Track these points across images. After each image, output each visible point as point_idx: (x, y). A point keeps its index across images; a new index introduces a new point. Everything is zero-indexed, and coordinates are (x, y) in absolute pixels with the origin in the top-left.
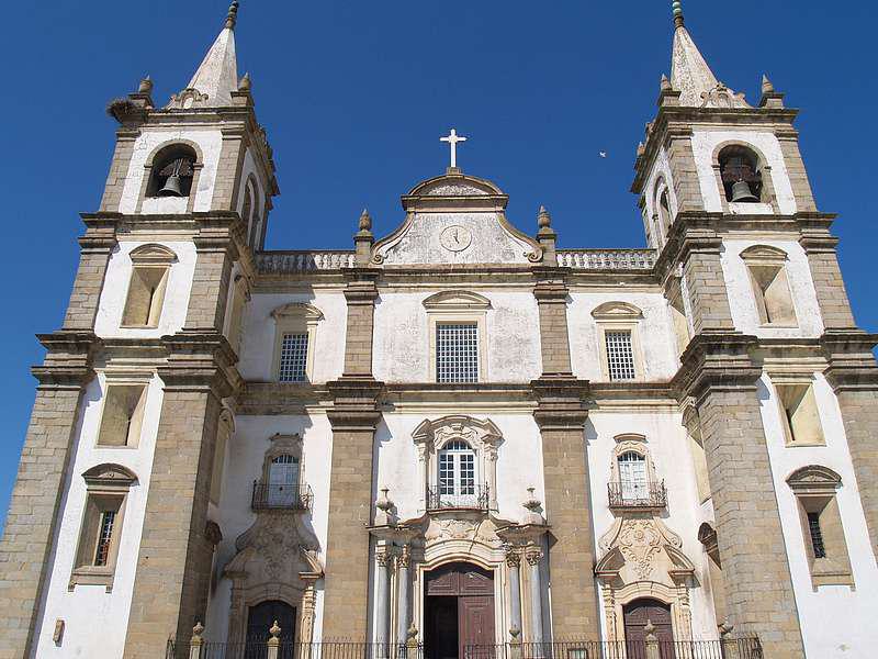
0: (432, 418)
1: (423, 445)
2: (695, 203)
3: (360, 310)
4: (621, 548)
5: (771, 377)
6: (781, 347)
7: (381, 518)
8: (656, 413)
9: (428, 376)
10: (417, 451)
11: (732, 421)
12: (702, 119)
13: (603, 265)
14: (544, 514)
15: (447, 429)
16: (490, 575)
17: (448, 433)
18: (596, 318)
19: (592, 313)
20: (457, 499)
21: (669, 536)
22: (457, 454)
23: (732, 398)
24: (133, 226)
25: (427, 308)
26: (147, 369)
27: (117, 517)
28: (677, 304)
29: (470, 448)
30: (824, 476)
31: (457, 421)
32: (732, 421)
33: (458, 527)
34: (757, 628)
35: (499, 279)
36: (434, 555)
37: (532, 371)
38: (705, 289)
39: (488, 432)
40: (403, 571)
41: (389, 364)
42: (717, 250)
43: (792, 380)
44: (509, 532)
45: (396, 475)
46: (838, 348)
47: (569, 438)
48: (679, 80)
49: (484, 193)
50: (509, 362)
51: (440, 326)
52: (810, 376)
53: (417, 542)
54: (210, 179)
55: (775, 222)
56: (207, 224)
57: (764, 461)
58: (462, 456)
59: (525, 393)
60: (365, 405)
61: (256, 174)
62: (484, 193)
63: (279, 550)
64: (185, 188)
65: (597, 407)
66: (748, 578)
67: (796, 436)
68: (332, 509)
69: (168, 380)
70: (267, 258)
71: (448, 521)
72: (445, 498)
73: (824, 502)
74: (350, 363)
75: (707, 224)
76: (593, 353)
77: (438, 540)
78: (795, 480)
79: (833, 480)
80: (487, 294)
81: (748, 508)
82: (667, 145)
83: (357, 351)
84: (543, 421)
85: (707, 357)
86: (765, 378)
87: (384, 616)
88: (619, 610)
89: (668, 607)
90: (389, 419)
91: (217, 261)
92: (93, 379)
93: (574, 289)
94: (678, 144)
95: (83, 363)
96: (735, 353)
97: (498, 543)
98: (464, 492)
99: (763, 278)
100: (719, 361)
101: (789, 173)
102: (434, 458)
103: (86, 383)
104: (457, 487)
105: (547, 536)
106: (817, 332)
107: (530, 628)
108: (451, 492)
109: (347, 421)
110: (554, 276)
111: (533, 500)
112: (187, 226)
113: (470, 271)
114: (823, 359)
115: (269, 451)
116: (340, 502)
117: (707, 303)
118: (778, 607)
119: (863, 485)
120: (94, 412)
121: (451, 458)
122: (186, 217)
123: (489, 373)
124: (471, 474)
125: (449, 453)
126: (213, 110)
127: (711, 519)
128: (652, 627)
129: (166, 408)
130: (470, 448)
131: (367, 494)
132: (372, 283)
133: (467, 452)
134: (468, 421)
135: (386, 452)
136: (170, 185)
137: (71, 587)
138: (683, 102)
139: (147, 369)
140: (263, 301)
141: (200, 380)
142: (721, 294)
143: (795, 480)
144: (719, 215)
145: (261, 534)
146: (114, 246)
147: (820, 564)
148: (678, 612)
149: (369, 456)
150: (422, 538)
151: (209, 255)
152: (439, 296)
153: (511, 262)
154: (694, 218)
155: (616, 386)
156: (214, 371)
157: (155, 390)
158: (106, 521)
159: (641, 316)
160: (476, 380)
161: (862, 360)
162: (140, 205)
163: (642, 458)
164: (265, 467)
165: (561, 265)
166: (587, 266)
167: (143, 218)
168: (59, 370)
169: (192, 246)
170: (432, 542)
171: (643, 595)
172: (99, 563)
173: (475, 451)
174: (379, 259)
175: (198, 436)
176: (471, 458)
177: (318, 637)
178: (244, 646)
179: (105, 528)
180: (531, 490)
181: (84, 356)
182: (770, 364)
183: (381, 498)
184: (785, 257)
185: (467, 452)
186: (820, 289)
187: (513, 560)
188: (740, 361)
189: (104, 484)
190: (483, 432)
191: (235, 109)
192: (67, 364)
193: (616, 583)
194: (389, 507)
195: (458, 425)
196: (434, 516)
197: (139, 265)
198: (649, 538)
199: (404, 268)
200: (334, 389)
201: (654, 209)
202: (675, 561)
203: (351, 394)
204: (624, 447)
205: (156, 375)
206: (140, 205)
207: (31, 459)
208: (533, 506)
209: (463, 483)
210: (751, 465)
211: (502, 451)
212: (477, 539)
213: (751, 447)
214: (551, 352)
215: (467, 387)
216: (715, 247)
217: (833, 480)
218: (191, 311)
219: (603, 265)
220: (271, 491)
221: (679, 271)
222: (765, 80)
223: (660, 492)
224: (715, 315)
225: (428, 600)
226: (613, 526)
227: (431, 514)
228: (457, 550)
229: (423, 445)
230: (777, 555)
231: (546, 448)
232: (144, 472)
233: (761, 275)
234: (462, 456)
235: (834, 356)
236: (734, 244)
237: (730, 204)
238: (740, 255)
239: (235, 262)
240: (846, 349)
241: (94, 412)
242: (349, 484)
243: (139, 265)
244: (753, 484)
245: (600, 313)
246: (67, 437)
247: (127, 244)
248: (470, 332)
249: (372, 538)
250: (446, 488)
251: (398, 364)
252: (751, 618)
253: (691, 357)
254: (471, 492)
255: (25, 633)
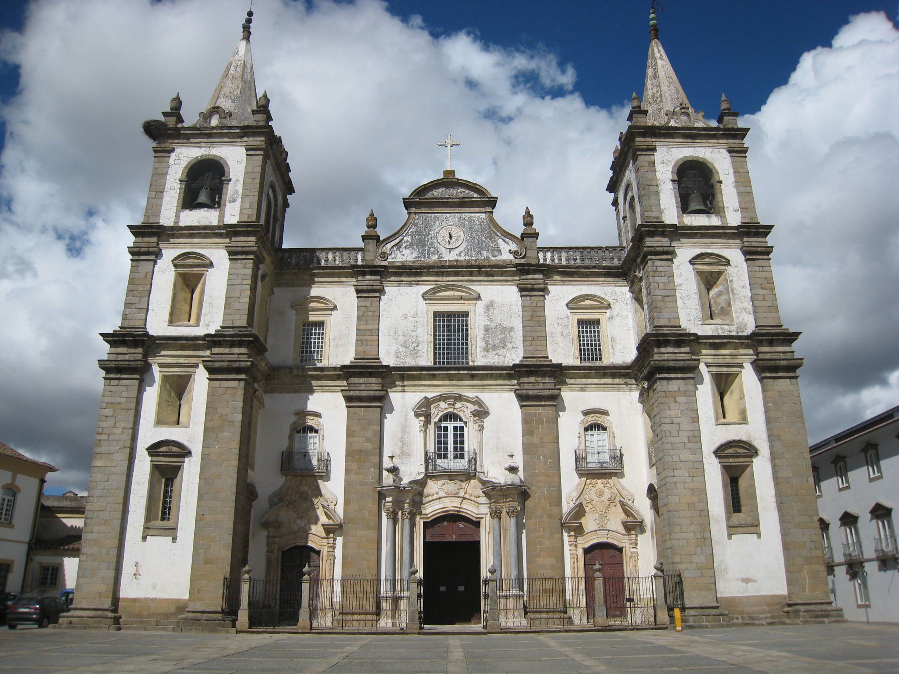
0: (430, 395)
1: (422, 418)
2: (654, 214)
3: (367, 302)
4: (584, 503)
5: (708, 367)
6: (717, 342)
7: (388, 479)
8: (618, 391)
9: (426, 359)
10: (416, 424)
11: (672, 405)
12: (666, 136)
13: (578, 261)
14: (521, 474)
15: (442, 405)
16: (477, 524)
17: (443, 407)
18: (570, 308)
19: (567, 305)
20: (450, 463)
21: (624, 493)
22: (451, 425)
23: (674, 386)
24: (174, 236)
25: (425, 299)
26: (193, 361)
27: (176, 482)
28: (638, 299)
29: (461, 420)
30: (745, 448)
31: (450, 398)
32: (672, 405)
33: (451, 486)
34: (682, 567)
35: (488, 274)
36: (431, 509)
37: (514, 356)
38: (658, 292)
39: (477, 408)
40: (407, 522)
41: (394, 348)
42: (669, 257)
43: (725, 369)
44: (493, 491)
45: (399, 444)
46: (764, 343)
47: (542, 411)
48: (650, 93)
49: (475, 195)
50: (495, 348)
51: (436, 314)
52: (741, 366)
53: (417, 499)
54: (237, 192)
55: (721, 233)
56: (236, 234)
57: (696, 437)
58: (454, 427)
59: (507, 374)
60: (372, 385)
61: (276, 184)
62: (475, 195)
63: (305, 506)
64: (215, 201)
65: (566, 384)
66: (677, 529)
67: (726, 415)
68: (348, 471)
69: (211, 370)
70: (287, 255)
71: (443, 482)
72: (440, 463)
73: (744, 468)
74: (361, 349)
75: (663, 234)
76: (567, 339)
77: (435, 497)
78: (720, 452)
79: (751, 451)
80: (477, 288)
81: (682, 474)
82: (635, 160)
83: (366, 337)
84: (523, 398)
85: (656, 350)
86: (702, 368)
87: (391, 631)
88: (580, 552)
89: (620, 550)
90: (395, 396)
91: (246, 268)
92: (149, 369)
93: (552, 282)
94: (643, 159)
95: (140, 357)
96: (679, 347)
97: (484, 499)
98: (456, 457)
99: (709, 280)
100: (665, 354)
101: (736, 187)
102: (431, 427)
103: (144, 373)
104: (451, 454)
105: (522, 493)
106: (750, 327)
107: (508, 565)
108: (445, 457)
109: (360, 399)
110: (536, 272)
111: (513, 465)
112: (220, 235)
113: (462, 267)
114: (751, 352)
115: (294, 423)
116: (354, 466)
117: (660, 304)
118: (698, 550)
119: (773, 458)
120: (151, 396)
121: (446, 429)
122: (218, 227)
123: (479, 357)
124: (463, 442)
125: (443, 424)
126: (237, 127)
127: (655, 482)
128: (601, 567)
129: (211, 394)
130: (461, 420)
131: (377, 459)
132: (378, 277)
133: (459, 424)
134: (460, 398)
135: (391, 423)
136: (203, 198)
137: (144, 538)
138: (650, 121)
139: (193, 361)
140: (283, 295)
141: (238, 371)
142: (671, 297)
143: (720, 452)
144: (673, 226)
145: (290, 492)
146: (158, 254)
147: (737, 518)
148: (629, 554)
149: (378, 428)
150: (421, 494)
151: (239, 261)
152: (434, 291)
153: (498, 258)
154: (658, 229)
155: (584, 368)
156: (249, 364)
157: (201, 380)
158: (166, 486)
159: (609, 306)
160: (467, 363)
161: (783, 353)
162: (177, 216)
163: (605, 429)
164: (291, 438)
165: (542, 262)
166: (564, 262)
167: (182, 228)
168: (122, 363)
169: (224, 253)
170: (430, 498)
171: (600, 540)
172: (163, 519)
173: (466, 423)
174: (384, 256)
175: (239, 417)
176: (462, 429)
177: (338, 573)
178: (279, 582)
179: (166, 491)
180: (512, 456)
181: (140, 350)
182: (706, 356)
183: (387, 463)
184: (728, 263)
185: (459, 424)
186: (754, 291)
187: (496, 514)
188: (681, 354)
189: (165, 456)
190: (472, 407)
191: (257, 127)
192: (127, 357)
193: (579, 531)
194: (394, 470)
195: (452, 401)
196: (432, 477)
197: (181, 270)
198: (607, 495)
199: (406, 264)
200: (346, 372)
201: (625, 210)
202: (627, 512)
203: (361, 375)
204: (590, 419)
205: (201, 366)
206: (177, 216)
207: (104, 437)
208: (513, 470)
209: (456, 449)
210: (686, 440)
211: (487, 422)
212: (467, 496)
213: (686, 426)
214: (530, 338)
215: (459, 369)
216: (670, 254)
217: (751, 451)
218: (228, 311)
219: (578, 261)
220: (296, 457)
221: (640, 274)
222: (724, 98)
223: (618, 458)
224: (665, 313)
225: (426, 545)
226: (578, 485)
227: (428, 476)
228: (451, 505)
229: (422, 418)
230: (701, 511)
231: (526, 421)
232: (197, 448)
233: (707, 277)
234: (454, 427)
235: (761, 349)
236: (685, 251)
237: (684, 215)
238: (690, 261)
239: (261, 265)
240: (771, 343)
241: (151, 396)
242: (360, 451)
243: (181, 270)
244: (686, 455)
245: (574, 304)
246: (132, 418)
247: (169, 253)
248: (463, 320)
249: (381, 496)
250: (441, 453)
251: (401, 349)
252: (677, 559)
253: (647, 345)
254: (462, 457)
255: (112, 573)
